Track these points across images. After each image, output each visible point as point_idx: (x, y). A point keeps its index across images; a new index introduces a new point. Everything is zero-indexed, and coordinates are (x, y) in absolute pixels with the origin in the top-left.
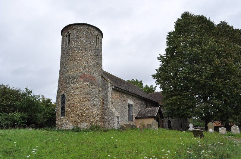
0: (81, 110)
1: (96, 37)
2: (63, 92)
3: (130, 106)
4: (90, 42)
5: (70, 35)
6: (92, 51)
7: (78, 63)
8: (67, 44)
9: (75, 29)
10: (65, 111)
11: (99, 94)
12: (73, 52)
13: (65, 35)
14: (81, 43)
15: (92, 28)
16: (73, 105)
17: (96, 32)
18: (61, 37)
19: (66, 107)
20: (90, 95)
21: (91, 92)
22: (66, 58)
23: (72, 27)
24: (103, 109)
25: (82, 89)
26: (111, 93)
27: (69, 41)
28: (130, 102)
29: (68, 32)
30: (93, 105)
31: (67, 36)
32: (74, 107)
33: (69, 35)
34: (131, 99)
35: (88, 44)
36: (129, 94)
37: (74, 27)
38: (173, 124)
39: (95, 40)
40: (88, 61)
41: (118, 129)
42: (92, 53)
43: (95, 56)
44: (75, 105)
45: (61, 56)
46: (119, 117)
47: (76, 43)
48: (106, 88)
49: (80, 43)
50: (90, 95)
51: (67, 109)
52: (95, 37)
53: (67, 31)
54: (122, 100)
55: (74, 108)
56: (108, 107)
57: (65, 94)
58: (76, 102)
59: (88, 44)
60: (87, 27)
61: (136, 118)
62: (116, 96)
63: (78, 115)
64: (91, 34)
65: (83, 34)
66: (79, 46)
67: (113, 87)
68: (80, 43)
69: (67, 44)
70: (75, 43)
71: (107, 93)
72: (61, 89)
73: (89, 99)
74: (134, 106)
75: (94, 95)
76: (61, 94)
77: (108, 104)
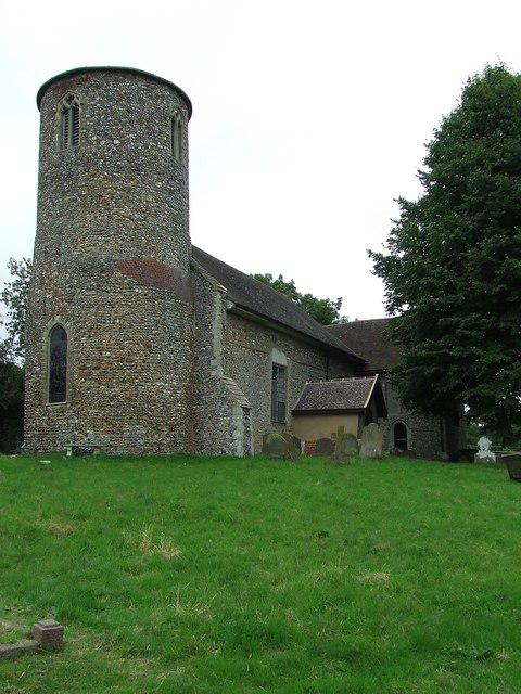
0: (124, 381)
1: (173, 122)
3: (278, 370)
4: (153, 142)
7: (110, 217)
8: (69, 144)
10: (68, 383)
12: (94, 175)
13: (60, 107)
14: (123, 143)
17: (173, 104)
21: (157, 322)
22: (64, 194)
23: (87, 80)
24: (194, 380)
27: (76, 131)
29: (71, 98)
30: (162, 367)
31: (65, 112)
32: (101, 370)
33: (75, 110)
37: (95, 81)
39: (169, 133)
42: (158, 180)
49: (117, 142)
51: (74, 377)
52: (170, 123)
54: (254, 351)
56: (213, 374)
57: (67, 326)
58: (108, 354)
59: (146, 146)
60: (141, 84)
61: (296, 414)
63: (112, 399)
64: (157, 109)
66: (113, 152)
69: (69, 144)
70: (98, 141)
71: (208, 327)
73: (148, 346)
74: (289, 372)
76: (50, 325)
77: (213, 363)
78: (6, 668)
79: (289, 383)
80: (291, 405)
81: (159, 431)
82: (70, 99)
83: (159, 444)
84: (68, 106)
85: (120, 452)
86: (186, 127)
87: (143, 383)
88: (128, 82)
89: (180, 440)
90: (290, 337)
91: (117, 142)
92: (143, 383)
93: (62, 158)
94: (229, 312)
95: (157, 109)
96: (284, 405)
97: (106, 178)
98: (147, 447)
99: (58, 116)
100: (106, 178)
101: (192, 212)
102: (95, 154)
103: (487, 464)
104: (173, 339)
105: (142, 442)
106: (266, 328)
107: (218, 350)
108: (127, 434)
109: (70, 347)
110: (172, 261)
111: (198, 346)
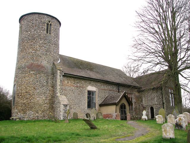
0: (27, 99)
1: (48, 24)
6: (41, 39)
9: (26, 19)
11: (47, 82)
12: (24, 43)
15: (42, 16)
18: (19, 24)
20: (36, 84)
21: (38, 81)
25: (29, 78)
26: (60, 80)
28: (91, 88)
30: (40, 94)
34: (92, 85)
35: (37, 32)
36: (89, 80)
38: (156, 110)
40: (36, 50)
41: (148, 120)
42: (40, 41)
43: (45, 44)
44: (23, 94)
45: (19, 45)
46: (67, 105)
47: (26, 34)
50: (36, 84)
52: (46, 25)
53: (22, 19)
55: (22, 97)
59: (37, 32)
60: (37, 16)
61: (101, 105)
62: (70, 84)
63: (24, 104)
64: (41, 22)
65: (33, 24)
67: (63, 74)
68: (29, 32)
73: (35, 88)
75: (41, 84)
78: (189, 77)
79: (97, 96)
80: (98, 100)
81: (38, 113)
83: (38, 117)
85: (25, 119)
86: (59, 29)
87: (33, 99)
88: (33, 16)
89: (45, 115)
91: (29, 32)
92: (33, 99)
94: (63, 76)
95: (41, 22)
97: (26, 43)
98: (34, 117)
100: (26, 43)
101: (18, 34)
103: (160, 69)
104: (43, 86)
105: (32, 116)
106: (99, 82)
108: (28, 114)
110: (45, 63)
111: (54, 86)
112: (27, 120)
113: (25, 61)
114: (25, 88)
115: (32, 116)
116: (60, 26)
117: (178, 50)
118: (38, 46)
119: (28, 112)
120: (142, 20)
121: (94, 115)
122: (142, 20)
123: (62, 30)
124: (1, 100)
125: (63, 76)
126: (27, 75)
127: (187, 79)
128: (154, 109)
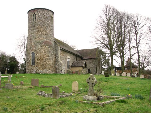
0: (44, 61)
2: (33, 51)
5: (36, 15)
9: (39, 11)
16: (40, 59)
19: (35, 60)
23: (38, 10)
24: (55, 61)
27: (35, 19)
30: (51, 59)
33: (35, 15)
35: (47, 22)
42: (50, 27)
44: (41, 59)
48: (57, 49)
49: (43, 21)
55: (41, 60)
57: (34, 52)
59: (47, 22)
60: (47, 11)
62: (62, 53)
63: (43, 64)
64: (49, 15)
65: (45, 16)
68: (43, 21)
72: (31, 49)
76: (32, 52)
82: (34, 13)
84: (34, 14)
90: (70, 53)
93: (33, 23)
94: (61, 50)
96: (69, 65)
99: (32, 16)
102: (39, 23)
105: (47, 71)
107: (59, 56)
108: (45, 70)
109: (35, 56)
111: (56, 56)
112: (45, 74)
113: (42, 39)
114: (42, 55)
115: (47, 71)
116: (53, 13)
117: (113, 45)
118: (48, 31)
119: (45, 70)
120: (101, 42)
121: (85, 72)
122: (101, 42)
123: (55, 17)
124: (133, 73)
125: (61, 50)
126: (44, 47)
127: (117, 56)
128: (91, 70)
